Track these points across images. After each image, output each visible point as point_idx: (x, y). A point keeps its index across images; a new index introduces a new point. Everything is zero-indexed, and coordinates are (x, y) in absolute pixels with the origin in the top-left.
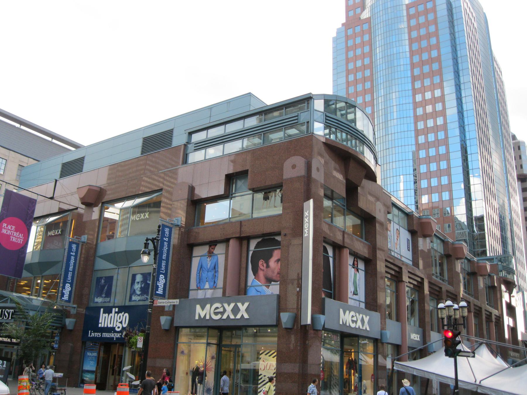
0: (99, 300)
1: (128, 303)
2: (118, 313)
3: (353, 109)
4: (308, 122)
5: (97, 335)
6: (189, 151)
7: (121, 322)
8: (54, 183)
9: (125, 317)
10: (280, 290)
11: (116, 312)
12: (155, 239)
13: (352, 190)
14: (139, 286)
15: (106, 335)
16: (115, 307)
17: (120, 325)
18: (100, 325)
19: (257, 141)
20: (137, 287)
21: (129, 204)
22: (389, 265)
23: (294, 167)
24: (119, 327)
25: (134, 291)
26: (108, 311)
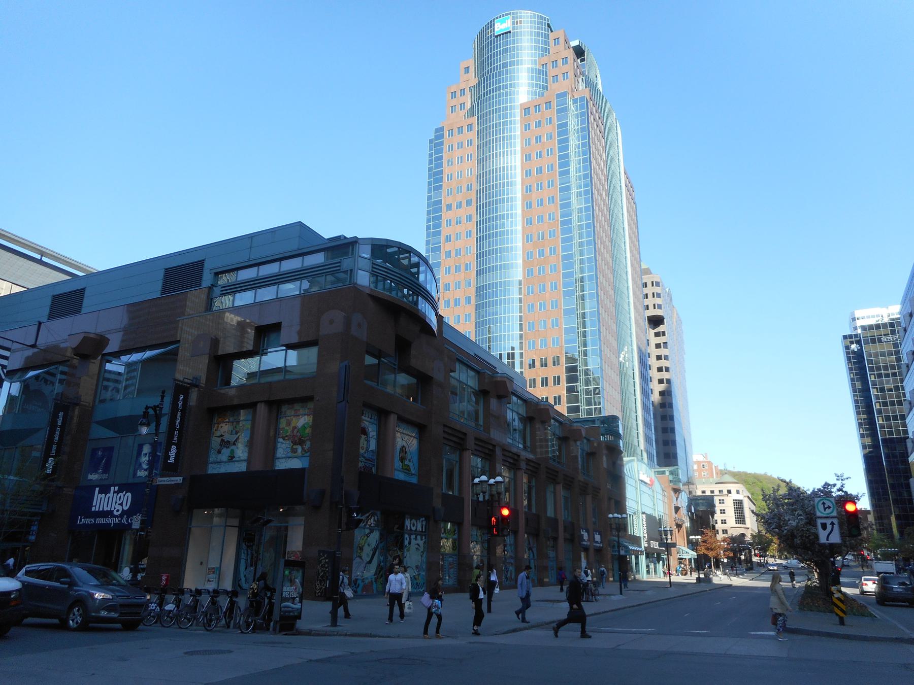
0: (93, 477)
1: (130, 481)
2: (118, 492)
4: (351, 270)
5: (88, 521)
6: (214, 295)
7: (121, 504)
8: (36, 327)
9: (127, 498)
10: (310, 463)
11: (115, 492)
12: (158, 406)
13: (403, 346)
14: (147, 458)
15: (100, 521)
16: (115, 486)
17: (120, 508)
18: (93, 509)
19: (306, 284)
21: (136, 357)
23: (332, 322)
24: (118, 511)
25: (140, 464)
26: (105, 490)
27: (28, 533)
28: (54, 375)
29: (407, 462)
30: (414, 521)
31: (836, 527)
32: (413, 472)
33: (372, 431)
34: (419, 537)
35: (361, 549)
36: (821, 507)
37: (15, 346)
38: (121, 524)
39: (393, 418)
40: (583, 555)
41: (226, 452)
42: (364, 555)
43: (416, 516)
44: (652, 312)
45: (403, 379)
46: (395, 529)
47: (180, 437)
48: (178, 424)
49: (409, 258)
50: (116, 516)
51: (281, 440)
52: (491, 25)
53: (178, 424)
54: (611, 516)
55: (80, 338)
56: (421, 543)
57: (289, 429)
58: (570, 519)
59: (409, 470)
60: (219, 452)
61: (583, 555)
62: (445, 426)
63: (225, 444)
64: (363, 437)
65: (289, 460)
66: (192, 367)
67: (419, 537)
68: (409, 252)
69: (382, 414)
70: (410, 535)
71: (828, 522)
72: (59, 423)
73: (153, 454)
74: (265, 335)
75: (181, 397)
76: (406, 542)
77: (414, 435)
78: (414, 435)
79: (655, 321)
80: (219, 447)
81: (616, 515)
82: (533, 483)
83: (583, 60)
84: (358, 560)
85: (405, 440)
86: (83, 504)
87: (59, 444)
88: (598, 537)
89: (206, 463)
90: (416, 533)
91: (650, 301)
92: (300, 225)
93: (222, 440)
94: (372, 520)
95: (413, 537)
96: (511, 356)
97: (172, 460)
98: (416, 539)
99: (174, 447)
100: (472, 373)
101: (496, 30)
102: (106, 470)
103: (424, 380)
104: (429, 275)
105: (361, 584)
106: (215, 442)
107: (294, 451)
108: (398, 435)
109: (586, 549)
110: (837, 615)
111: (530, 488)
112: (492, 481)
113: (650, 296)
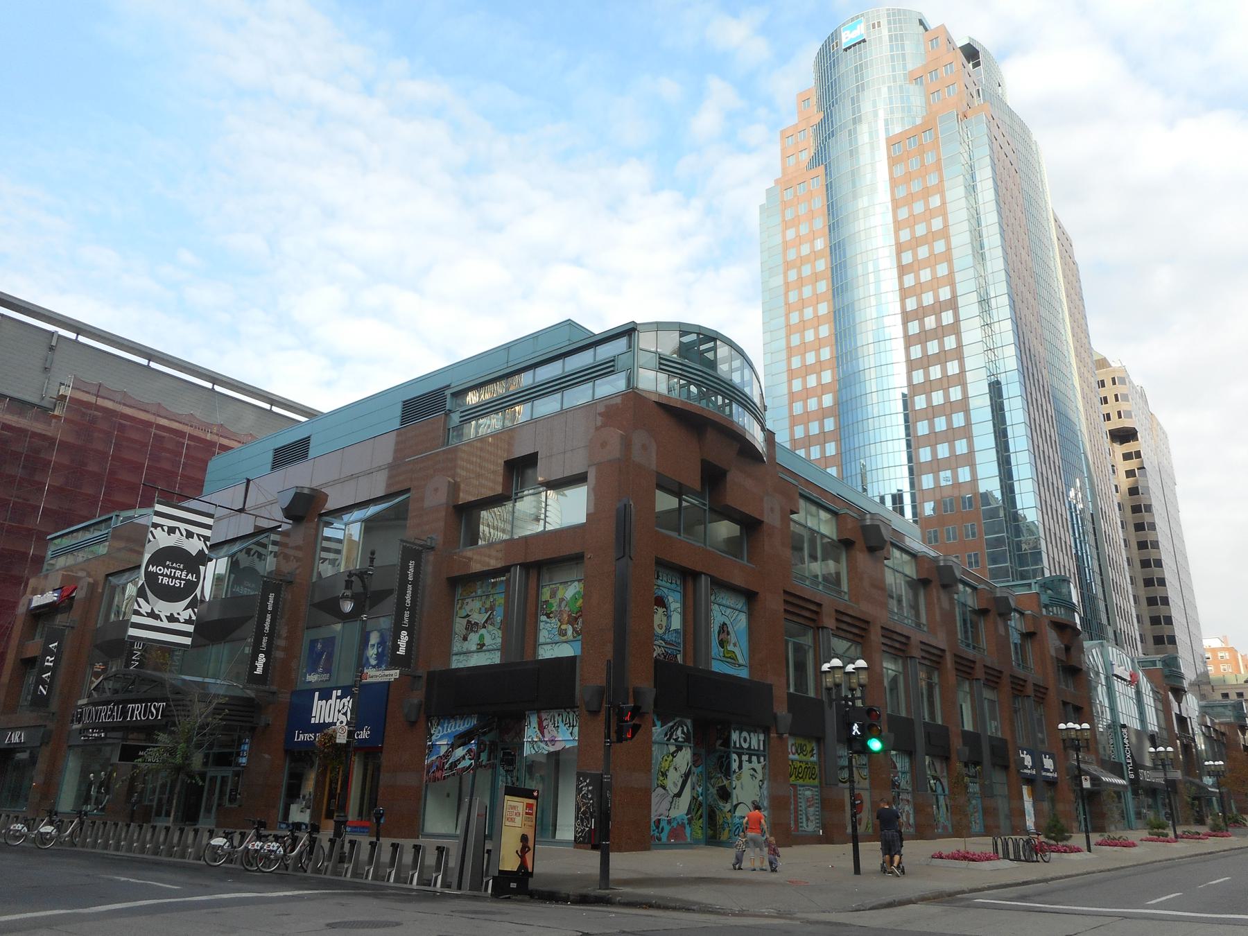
0: (312, 678)
3: (712, 344)
11: (337, 697)
13: (713, 477)
16: (337, 689)
20: (372, 652)
22: (790, 599)
26: (326, 696)
27: (238, 755)
28: (265, 546)
29: (731, 648)
30: (745, 734)
32: (741, 661)
34: (754, 758)
35: (664, 775)
37: (219, 512)
40: (1025, 790)
41: (474, 638)
42: (669, 783)
43: (753, 727)
44: (1116, 424)
45: (725, 529)
46: (718, 747)
48: (408, 601)
49: (714, 349)
51: (544, 618)
52: (833, 38)
53: (408, 601)
54: (1062, 726)
56: (759, 767)
58: (999, 735)
59: (734, 658)
60: (465, 639)
61: (1025, 790)
62: (785, 592)
63: (472, 627)
64: (661, 610)
65: (555, 644)
66: (429, 525)
67: (754, 758)
68: (714, 340)
69: (688, 576)
70: (740, 756)
73: (382, 643)
74: (519, 470)
75: (412, 564)
76: (735, 766)
79: (1124, 435)
80: (464, 632)
81: (1070, 725)
82: (936, 679)
83: (977, 65)
84: (660, 790)
85: (729, 615)
86: (300, 715)
87: (271, 635)
88: (1048, 763)
89: (448, 654)
90: (751, 752)
91: (1111, 408)
92: (569, 323)
93: (469, 622)
95: (745, 758)
96: (898, 499)
97: (259, 671)
98: (750, 761)
99: (404, 633)
100: (824, 515)
102: (327, 670)
103: (751, 526)
104: (747, 372)
105: (667, 828)
106: (459, 625)
107: (563, 633)
108: (715, 607)
109: (1030, 781)
111: (930, 687)
112: (850, 668)
113: (1111, 399)
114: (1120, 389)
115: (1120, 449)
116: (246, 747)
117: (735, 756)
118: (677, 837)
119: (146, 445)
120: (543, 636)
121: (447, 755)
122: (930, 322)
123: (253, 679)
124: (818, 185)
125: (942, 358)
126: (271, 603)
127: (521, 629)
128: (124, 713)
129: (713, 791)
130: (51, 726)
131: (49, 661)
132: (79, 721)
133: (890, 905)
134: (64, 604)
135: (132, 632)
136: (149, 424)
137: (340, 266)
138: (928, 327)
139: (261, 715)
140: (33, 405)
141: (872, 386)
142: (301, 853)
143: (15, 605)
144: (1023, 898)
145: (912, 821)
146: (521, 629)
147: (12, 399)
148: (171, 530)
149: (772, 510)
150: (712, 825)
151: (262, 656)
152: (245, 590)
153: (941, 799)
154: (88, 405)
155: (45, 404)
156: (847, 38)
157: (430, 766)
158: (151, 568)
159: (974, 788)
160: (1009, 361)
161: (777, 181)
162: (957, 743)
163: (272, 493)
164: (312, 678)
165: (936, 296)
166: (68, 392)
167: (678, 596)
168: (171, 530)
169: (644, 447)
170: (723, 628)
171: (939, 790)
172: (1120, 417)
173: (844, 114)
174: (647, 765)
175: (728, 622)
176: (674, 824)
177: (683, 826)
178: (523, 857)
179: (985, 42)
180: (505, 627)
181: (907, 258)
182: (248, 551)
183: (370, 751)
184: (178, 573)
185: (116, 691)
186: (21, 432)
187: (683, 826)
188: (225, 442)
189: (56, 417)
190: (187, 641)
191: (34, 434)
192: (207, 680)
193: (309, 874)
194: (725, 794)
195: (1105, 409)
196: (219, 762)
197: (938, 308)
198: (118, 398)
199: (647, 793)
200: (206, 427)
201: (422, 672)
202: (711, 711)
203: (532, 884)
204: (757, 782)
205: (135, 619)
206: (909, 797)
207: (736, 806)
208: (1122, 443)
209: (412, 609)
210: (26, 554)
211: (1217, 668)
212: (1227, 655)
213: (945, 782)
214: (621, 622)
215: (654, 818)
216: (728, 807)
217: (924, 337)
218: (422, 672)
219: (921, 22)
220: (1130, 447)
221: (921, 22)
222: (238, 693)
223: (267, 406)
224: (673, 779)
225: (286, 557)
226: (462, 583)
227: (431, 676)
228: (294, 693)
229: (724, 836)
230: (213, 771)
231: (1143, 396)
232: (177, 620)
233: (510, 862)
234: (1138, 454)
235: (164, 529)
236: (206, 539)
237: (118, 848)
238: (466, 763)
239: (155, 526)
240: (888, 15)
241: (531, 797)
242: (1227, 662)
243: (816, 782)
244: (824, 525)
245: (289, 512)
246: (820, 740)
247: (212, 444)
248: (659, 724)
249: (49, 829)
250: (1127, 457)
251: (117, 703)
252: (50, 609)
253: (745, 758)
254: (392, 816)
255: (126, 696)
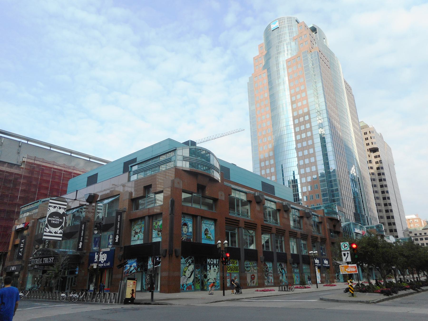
0: (95, 248)
17: (103, 260)
29: (209, 235)
31: (349, 255)
32: (212, 239)
33: (190, 224)
34: (215, 266)
35: (185, 272)
36: (343, 247)
38: (104, 266)
39: (199, 218)
41: (137, 236)
47: (119, 232)
50: (102, 263)
51: (154, 230)
52: (269, 26)
55: (88, 195)
56: (216, 269)
57: (156, 226)
60: (134, 236)
63: (136, 233)
64: (185, 227)
65: (156, 239)
67: (215, 266)
69: (194, 217)
70: (210, 266)
71: (346, 252)
72: (83, 229)
75: (119, 216)
76: (208, 269)
77: (212, 223)
78: (212, 223)
79: (374, 150)
84: (184, 276)
85: (208, 227)
87: (83, 237)
88: (326, 262)
89: (130, 241)
90: (214, 265)
91: (369, 141)
92: (169, 139)
94: (190, 260)
97: (80, 247)
98: (213, 267)
99: (81, 243)
100: (243, 194)
101: (272, 28)
105: (186, 287)
106: (133, 233)
107: (158, 235)
110: (350, 292)
113: (369, 138)
114: (372, 135)
115: (373, 155)
116: (77, 269)
117: (208, 266)
118: (189, 288)
119: (50, 175)
120: (154, 235)
121: (129, 269)
122: (301, 119)
123: (79, 249)
124: (265, 75)
125: (306, 131)
126: (81, 228)
127: (148, 235)
128: (42, 261)
129: (203, 276)
130: (23, 264)
131: (22, 246)
132: (30, 263)
133: (216, 302)
134: (26, 227)
135: (44, 237)
136: (51, 168)
137: (113, 109)
138: (301, 121)
139: (81, 259)
140: (15, 165)
141: (286, 140)
142: (83, 297)
143: (11, 227)
144: (257, 300)
145: (273, 281)
146: (148, 235)
147: (8, 163)
148: (55, 207)
149: (222, 195)
150: (201, 284)
151: (81, 243)
152: (78, 223)
153: (284, 275)
154: (32, 163)
155: (19, 164)
156: (273, 27)
157: (125, 272)
158: (49, 219)
159: (297, 271)
160: (326, 131)
161: (252, 74)
162: (289, 258)
163: (84, 192)
164: (95, 248)
165: (303, 111)
166: (25, 160)
167: (191, 222)
168: (55, 207)
169: (178, 183)
170: (206, 230)
171: (283, 272)
172: (372, 144)
173: (273, 52)
174: (179, 270)
175: (208, 228)
176: (188, 285)
177: (191, 286)
178: (132, 294)
179: (319, 25)
180: (144, 233)
181: (294, 99)
182: (78, 211)
183: (110, 268)
184: (57, 219)
185: (40, 254)
186: (11, 174)
187: (191, 286)
188: (75, 172)
189: (23, 168)
190: (61, 239)
191: (16, 174)
192: (67, 250)
193: (85, 302)
194: (206, 277)
195: (367, 142)
196: (71, 275)
197: (304, 115)
198: (41, 160)
199: (179, 278)
200: (69, 168)
201: (122, 246)
202: (200, 254)
203: (135, 301)
204: (216, 273)
205: (45, 234)
206: (272, 275)
207: (208, 280)
208: (374, 152)
209: (120, 229)
210: (14, 211)
211: (414, 225)
212: (417, 221)
213: (285, 269)
214: (172, 232)
215: (181, 284)
216: (206, 280)
217: (300, 124)
218: (122, 246)
219: (296, 21)
220: (376, 154)
221: (296, 21)
222: (76, 254)
223: (88, 159)
224: (188, 273)
225: (89, 212)
226: (133, 221)
227: (125, 247)
228: (90, 253)
229: (205, 288)
230: (69, 277)
231: (381, 136)
232: (57, 233)
233: (128, 296)
234: (379, 156)
235: (54, 207)
236: (65, 209)
237: (40, 298)
238: (134, 271)
239: (50, 206)
240: (287, 19)
241: (135, 280)
242: (417, 223)
243: (238, 272)
244: (243, 197)
245: (87, 201)
246: (239, 259)
247: (70, 173)
248: (183, 258)
249: (21, 294)
250: (376, 157)
251: (40, 258)
252: (22, 229)
253: (212, 266)
254: (116, 287)
255: (43, 256)
